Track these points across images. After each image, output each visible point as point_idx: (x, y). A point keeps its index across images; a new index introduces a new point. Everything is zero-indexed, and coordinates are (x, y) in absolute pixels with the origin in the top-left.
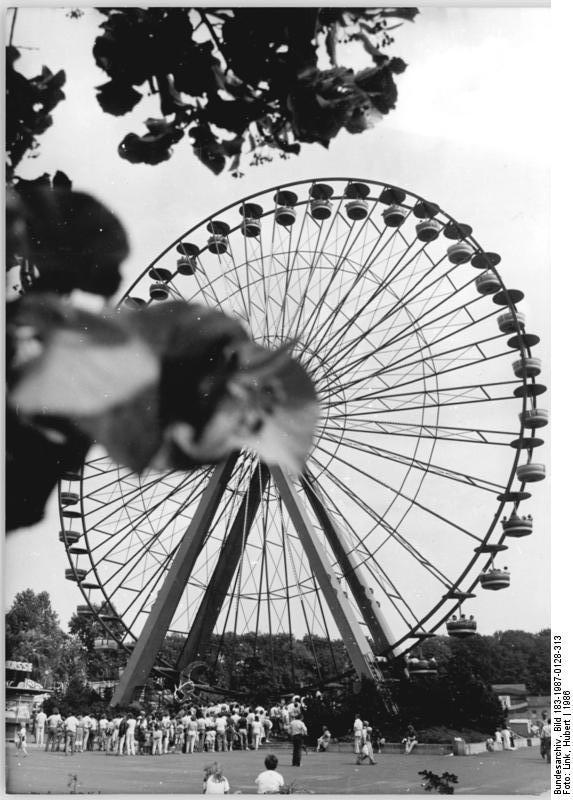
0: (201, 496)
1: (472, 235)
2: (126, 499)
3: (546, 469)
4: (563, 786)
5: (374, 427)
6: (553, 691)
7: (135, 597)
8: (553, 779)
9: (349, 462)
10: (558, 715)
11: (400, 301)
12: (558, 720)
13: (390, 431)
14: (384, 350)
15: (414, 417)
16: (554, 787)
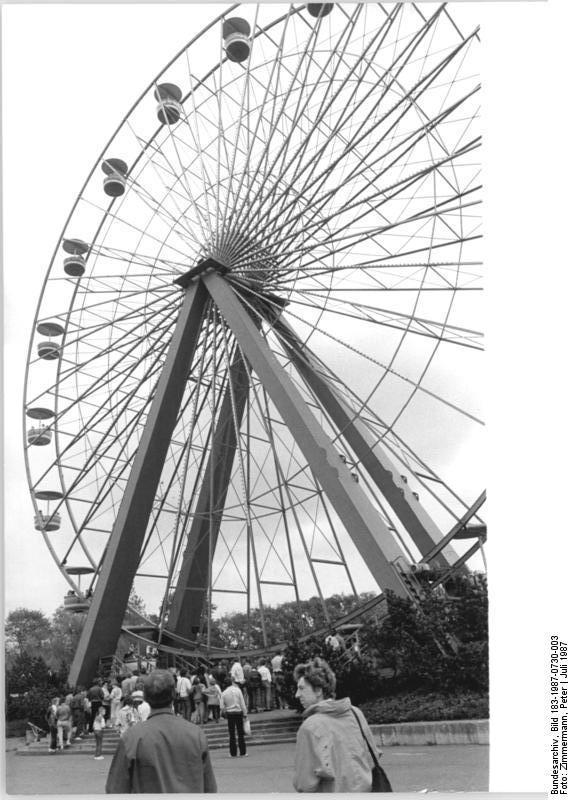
0: (161, 369)
2: (456, 203)
4: (560, 786)
7: (57, 553)
9: (194, 36)
13: (379, 320)
14: (75, 489)
15: (402, 303)
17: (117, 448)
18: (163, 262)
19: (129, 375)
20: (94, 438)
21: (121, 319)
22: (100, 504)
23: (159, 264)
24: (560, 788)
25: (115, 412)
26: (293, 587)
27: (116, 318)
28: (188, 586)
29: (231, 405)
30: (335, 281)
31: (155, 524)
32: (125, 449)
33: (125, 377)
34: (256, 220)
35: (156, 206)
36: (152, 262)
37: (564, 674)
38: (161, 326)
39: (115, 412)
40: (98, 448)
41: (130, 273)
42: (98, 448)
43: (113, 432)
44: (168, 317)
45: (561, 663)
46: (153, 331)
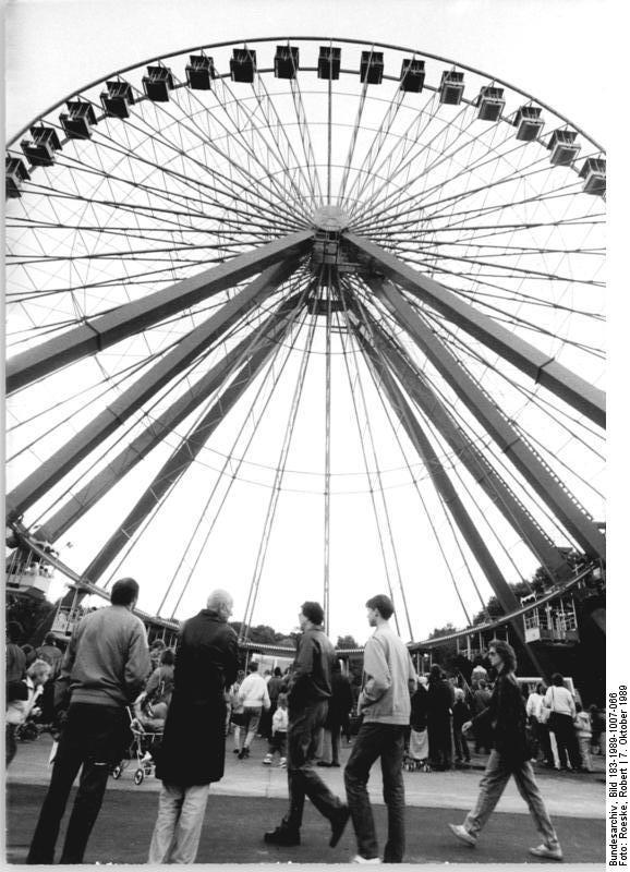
4: (619, 856)
5: (353, 373)
6: (608, 754)
8: (609, 850)
10: (613, 780)
11: (534, 394)
16: (609, 858)
18: (315, 171)
19: (181, 231)
23: (312, 169)
24: (619, 859)
28: (602, 859)
30: (70, 242)
34: (384, 236)
35: (385, 130)
36: (311, 163)
41: (285, 127)
45: (620, 766)
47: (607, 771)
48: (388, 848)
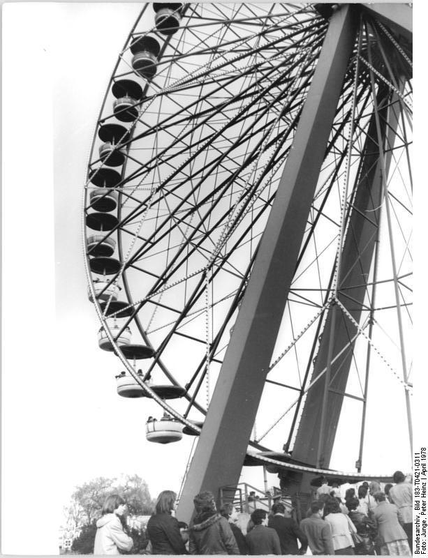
1: (411, 80)
3: (81, 261)
4: (421, 548)
10: (418, 499)
12: (418, 502)
17: (187, 188)
19: (223, 87)
20: (165, 171)
21: (239, 22)
22: (154, 244)
25: (194, 149)
26: (362, 403)
27: (236, 18)
29: (387, 38)
31: (186, 258)
32: (196, 192)
33: (218, 86)
37: (424, 472)
38: (276, 45)
39: (194, 149)
40: (167, 182)
42: (167, 182)
43: (186, 170)
44: (289, 37)
45: (421, 462)
46: (266, 48)
47: (414, 494)
48: (282, 545)
